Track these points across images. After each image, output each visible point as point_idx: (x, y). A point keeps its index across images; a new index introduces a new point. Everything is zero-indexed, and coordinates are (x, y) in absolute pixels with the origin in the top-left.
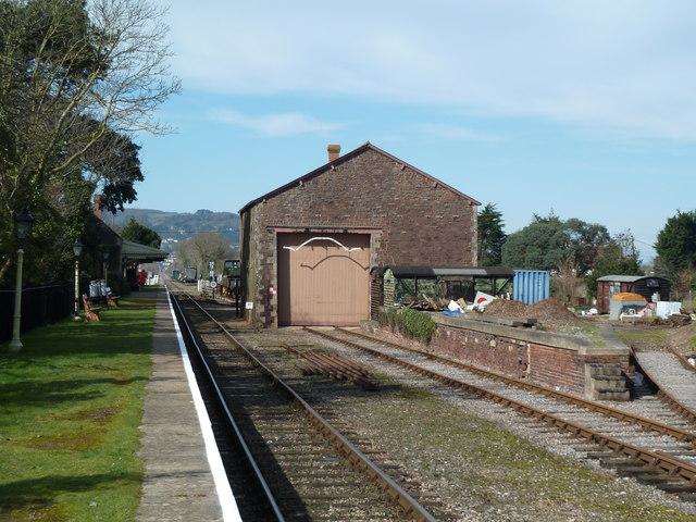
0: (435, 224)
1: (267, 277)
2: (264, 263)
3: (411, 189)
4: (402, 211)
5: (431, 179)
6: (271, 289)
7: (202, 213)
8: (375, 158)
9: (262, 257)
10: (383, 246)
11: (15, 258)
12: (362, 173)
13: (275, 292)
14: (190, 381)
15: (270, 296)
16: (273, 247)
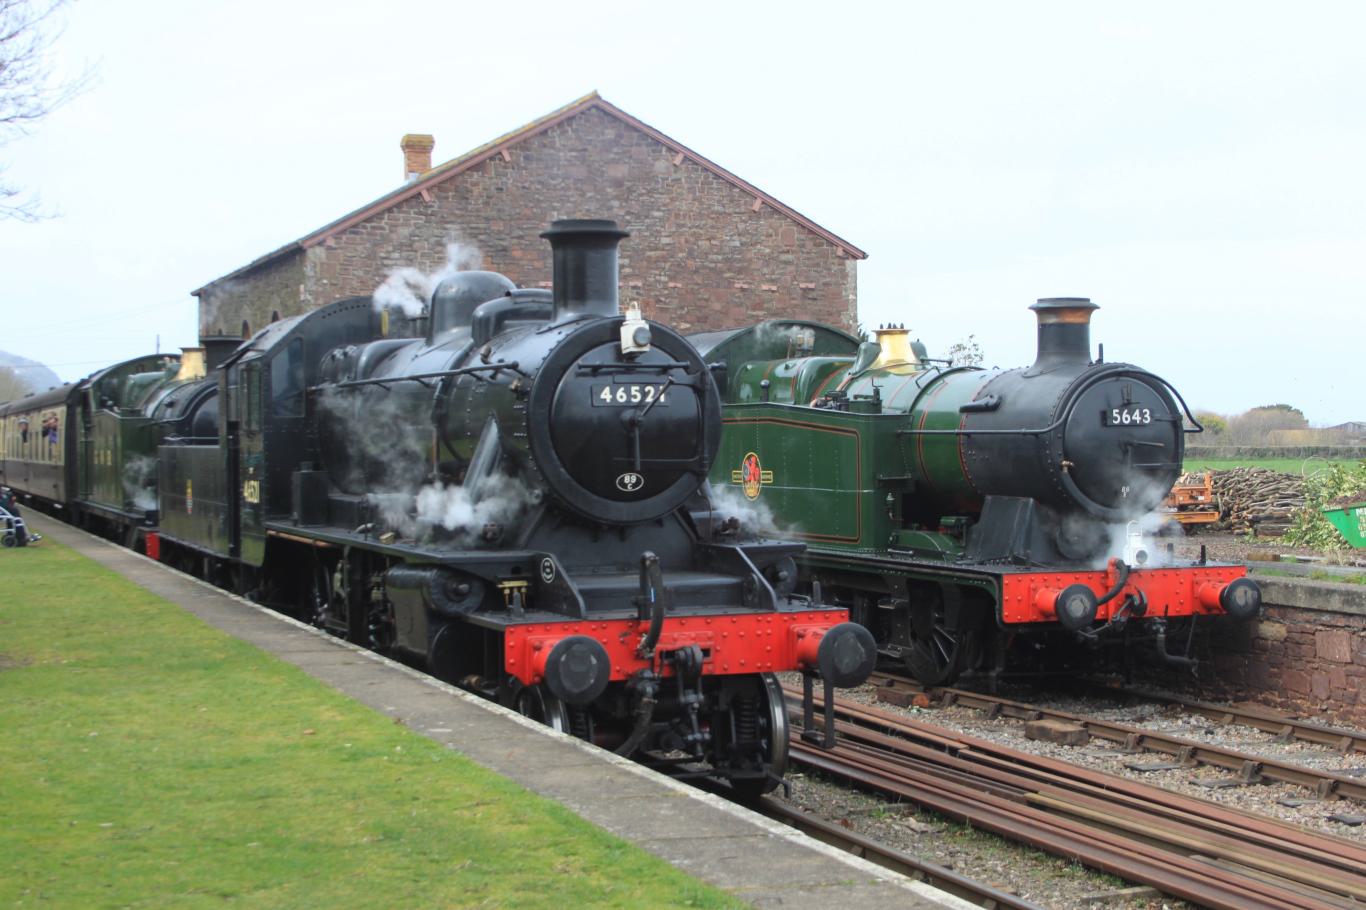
0: (757, 306)
3: (700, 215)
5: (749, 192)
8: (610, 134)
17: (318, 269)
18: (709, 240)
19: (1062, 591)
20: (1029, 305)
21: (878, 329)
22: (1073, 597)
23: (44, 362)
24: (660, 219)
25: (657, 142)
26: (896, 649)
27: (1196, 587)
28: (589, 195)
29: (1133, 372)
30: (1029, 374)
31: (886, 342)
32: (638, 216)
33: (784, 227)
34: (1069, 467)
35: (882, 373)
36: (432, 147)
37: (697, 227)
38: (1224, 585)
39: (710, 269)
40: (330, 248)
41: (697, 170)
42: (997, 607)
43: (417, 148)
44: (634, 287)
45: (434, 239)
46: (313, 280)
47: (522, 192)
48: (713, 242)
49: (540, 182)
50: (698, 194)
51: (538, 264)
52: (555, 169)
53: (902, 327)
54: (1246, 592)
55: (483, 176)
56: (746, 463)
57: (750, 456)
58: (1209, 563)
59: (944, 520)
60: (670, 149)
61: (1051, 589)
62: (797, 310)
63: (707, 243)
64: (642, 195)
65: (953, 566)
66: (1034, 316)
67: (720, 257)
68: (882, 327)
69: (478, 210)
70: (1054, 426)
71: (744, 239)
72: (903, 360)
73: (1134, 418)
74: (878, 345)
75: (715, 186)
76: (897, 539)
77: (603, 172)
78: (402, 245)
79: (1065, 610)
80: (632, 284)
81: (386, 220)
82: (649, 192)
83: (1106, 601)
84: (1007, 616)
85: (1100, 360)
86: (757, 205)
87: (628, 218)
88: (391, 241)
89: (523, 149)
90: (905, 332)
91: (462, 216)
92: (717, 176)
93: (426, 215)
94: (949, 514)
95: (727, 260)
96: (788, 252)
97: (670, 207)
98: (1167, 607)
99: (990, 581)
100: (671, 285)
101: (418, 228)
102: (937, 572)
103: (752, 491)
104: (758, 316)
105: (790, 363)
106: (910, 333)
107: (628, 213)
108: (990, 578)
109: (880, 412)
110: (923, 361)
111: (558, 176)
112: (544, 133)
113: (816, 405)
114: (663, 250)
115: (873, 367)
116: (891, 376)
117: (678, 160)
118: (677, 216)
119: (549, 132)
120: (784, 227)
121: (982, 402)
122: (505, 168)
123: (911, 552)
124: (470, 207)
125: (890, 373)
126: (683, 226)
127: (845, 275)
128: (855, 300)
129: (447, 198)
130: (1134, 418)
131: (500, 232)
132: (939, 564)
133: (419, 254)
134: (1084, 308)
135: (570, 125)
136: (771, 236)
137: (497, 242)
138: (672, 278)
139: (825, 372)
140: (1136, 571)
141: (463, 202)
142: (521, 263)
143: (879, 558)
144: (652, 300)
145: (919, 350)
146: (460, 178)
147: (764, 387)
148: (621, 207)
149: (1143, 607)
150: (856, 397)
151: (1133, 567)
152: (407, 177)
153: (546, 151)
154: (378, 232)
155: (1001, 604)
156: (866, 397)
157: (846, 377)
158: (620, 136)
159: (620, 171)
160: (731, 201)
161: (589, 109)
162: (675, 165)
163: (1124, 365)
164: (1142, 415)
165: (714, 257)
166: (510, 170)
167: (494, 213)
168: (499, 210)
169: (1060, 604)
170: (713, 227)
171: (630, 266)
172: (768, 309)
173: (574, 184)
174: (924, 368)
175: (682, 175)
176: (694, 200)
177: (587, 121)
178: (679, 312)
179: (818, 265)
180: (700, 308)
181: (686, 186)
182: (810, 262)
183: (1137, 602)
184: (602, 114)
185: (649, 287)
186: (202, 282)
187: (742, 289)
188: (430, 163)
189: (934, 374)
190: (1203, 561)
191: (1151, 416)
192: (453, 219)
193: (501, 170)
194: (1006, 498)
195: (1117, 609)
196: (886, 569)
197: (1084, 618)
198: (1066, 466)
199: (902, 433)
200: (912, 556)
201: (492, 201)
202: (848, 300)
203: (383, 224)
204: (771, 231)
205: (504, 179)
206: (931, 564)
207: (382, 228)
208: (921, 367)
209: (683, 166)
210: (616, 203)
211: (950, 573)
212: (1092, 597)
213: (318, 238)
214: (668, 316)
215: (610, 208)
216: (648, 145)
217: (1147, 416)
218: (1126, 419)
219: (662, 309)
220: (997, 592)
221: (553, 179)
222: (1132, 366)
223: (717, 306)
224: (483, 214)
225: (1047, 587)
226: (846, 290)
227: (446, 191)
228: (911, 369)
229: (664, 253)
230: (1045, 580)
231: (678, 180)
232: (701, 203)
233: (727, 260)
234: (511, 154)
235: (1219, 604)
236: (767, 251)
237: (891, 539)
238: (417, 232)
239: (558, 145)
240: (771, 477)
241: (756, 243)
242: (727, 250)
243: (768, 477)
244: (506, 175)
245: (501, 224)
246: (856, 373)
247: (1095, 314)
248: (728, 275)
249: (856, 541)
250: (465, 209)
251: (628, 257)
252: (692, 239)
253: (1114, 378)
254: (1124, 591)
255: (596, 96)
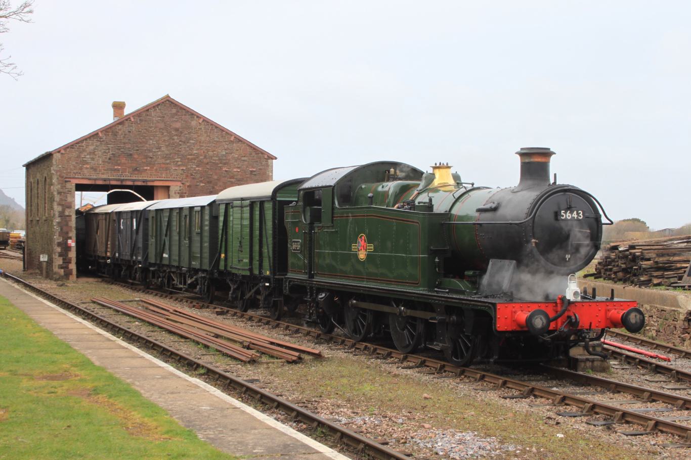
0: (232, 177)
1: (65, 229)
3: (209, 142)
5: (229, 133)
6: (70, 241)
8: (174, 111)
11: (461, 337)
12: (162, 125)
14: (175, 369)
15: (67, 248)
17: (58, 162)
18: (213, 152)
19: (530, 313)
20: (516, 152)
21: (434, 165)
22: (536, 317)
24: (193, 143)
25: (193, 114)
26: (438, 345)
27: (608, 313)
28: (165, 134)
29: (573, 190)
30: (515, 191)
31: (438, 173)
32: (184, 142)
33: (243, 147)
34: (536, 243)
35: (436, 190)
36: (124, 107)
37: (208, 147)
38: (624, 311)
39: (213, 163)
40: (62, 154)
41: (208, 125)
42: (493, 321)
43: (118, 107)
44: (182, 170)
45: (103, 151)
46: (56, 166)
47: (138, 133)
48: (214, 153)
49: (145, 129)
50: (209, 134)
51: (144, 160)
52: (151, 124)
53: (447, 164)
54: (636, 316)
55: (123, 127)
56: (359, 240)
57: (362, 236)
58: (616, 299)
59: (466, 273)
60: (198, 117)
61: (524, 312)
62: (248, 179)
63: (212, 153)
64: (186, 134)
65: (470, 298)
66: (518, 157)
67: (217, 158)
68: (436, 164)
69: (121, 140)
70: (527, 219)
71: (227, 151)
72: (447, 183)
73: (573, 216)
74: (433, 174)
75: (215, 131)
76: (440, 283)
77: (171, 125)
78: (90, 152)
79: (531, 324)
80: (181, 168)
81: (84, 143)
82: (189, 133)
83: (555, 319)
84: (499, 327)
85: (555, 183)
86: (232, 139)
87: (180, 143)
88: (87, 151)
89: (139, 116)
90: (449, 167)
91: (115, 142)
92: (216, 127)
93: (100, 141)
94: (469, 269)
95: (220, 159)
96: (245, 156)
97: (197, 139)
98: (591, 323)
99: (490, 307)
100: (197, 169)
101: (97, 146)
102: (461, 301)
103: (362, 255)
104: (232, 181)
105: (385, 184)
106: (452, 168)
107: (180, 141)
108: (490, 305)
109: (432, 211)
110: (458, 183)
111: (152, 126)
112: (148, 110)
113: (398, 208)
114: (194, 155)
115: (431, 186)
116: (441, 192)
117: (201, 121)
118: (200, 142)
119: (150, 110)
120: (243, 147)
121: (488, 206)
122: (132, 123)
123: (447, 290)
124: (118, 139)
125: (440, 190)
126: (202, 146)
127: (268, 165)
128: (272, 176)
129: (108, 135)
130: (573, 216)
131: (129, 148)
132: (462, 297)
133: (97, 156)
134: (546, 154)
135: (158, 107)
136: (238, 150)
137: (129, 152)
138: (198, 166)
139: (404, 189)
140: (573, 303)
141: (115, 136)
142: (138, 160)
143: (430, 294)
144: (189, 175)
145: (456, 177)
146: (114, 128)
147: (370, 197)
148: (178, 139)
149: (577, 323)
150: (419, 203)
151: (572, 300)
152: (114, 119)
153: (148, 117)
154: (81, 148)
155: (495, 321)
156: (425, 203)
157: (416, 192)
158: (178, 112)
159: (178, 125)
160: (222, 137)
161: (165, 101)
162: (199, 123)
163: (568, 186)
164: (578, 214)
165: (215, 158)
166: (133, 125)
167: (127, 141)
168: (129, 140)
169: (529, 320)
170: (214, 147)
171: (181, 161)
172: (236, 179)
173: (159, 130)
174: (459, 187)
175: (202, 127)
176: (207, 136)
177: (165, 106)
178: (200, 179)
179: (257, 162)
180: (208, 178)
181: (204, 131)
182: (254, 160)
183: (574, 321)
184: (170, 103)
185: (188, 170)
186: (26, 161)
187: (226, 171)
188: (123, 112)
189: (463, 190)
190: (612, 297)
191: (583, 214)
192: (110, 143)
193: (130, 124)
195: (562, 324)
196: (433, 299)
197: (542, 328)
198: (534, 242)
199: (444, 223)
200: (448, 293)
201: (127, 136)
202: (269, 175)
203: (83, 144)
204: (238, 148)
205: (131, 128)
206: (458, 297)
207: (83, 146)
208: (457, 187)
209: (203, 123)
210: (176, 137)
211: (468, 302)
212: (547, 316)
213: (59, 151)
214: (196, 181)
215: (173, 139)
216: (189, 115)
217: (581, 215)
218: (569, 216)
219: (193, 178)
220: (493, 313)
221: (150, 128)
222: (573, 186)
223: (216, 177)
224: (122, 141)
225: (522, 311)
226: (268, 171)
228: (452, 188)
229: (195, 156)
230: (521, 307)
231: (201, 129)
232: (210, 137)
233: (220, 159)
234: (134, 118)
235: (620, 320)
236: (237, 156)
237: (437, 283)
238: (97, 148)
239: (153, 115)
240: (372, 247)
241: (232, 153)
242: (220, 155)
243: (371, 247)
244: (132, 126)
245: (130, 145)
246: (421, 190)
247: (553, 158)
248: (220, 165)
249: (417, 284)
250: (116, 139)
251: (180, 158)
252: (206, 151)
253: (562, 193)
254: (566, 314)
255: (168, 96)
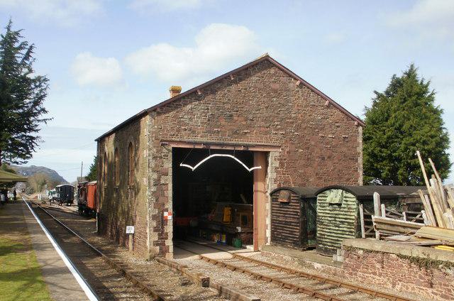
0: (327, 144)
2: (157, 183)
3: (306, 106)
4: (298, 128)
5: (324, 97)
6: (166, 214)
7: (436, 112)
9: (155, 176)
10: (282, 165)
13: (170, 218)
16: (168, 165)
23: (44, 166)
107: (279, 103)
194: (144, 118)
227: (207, 90)
